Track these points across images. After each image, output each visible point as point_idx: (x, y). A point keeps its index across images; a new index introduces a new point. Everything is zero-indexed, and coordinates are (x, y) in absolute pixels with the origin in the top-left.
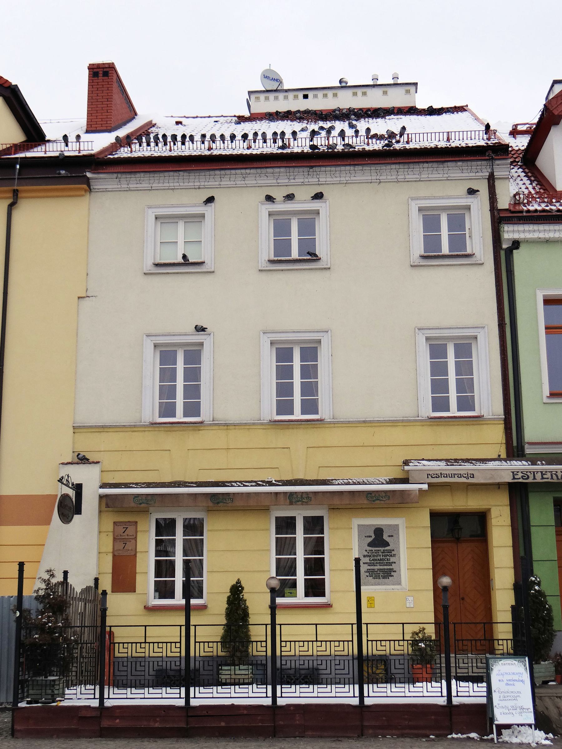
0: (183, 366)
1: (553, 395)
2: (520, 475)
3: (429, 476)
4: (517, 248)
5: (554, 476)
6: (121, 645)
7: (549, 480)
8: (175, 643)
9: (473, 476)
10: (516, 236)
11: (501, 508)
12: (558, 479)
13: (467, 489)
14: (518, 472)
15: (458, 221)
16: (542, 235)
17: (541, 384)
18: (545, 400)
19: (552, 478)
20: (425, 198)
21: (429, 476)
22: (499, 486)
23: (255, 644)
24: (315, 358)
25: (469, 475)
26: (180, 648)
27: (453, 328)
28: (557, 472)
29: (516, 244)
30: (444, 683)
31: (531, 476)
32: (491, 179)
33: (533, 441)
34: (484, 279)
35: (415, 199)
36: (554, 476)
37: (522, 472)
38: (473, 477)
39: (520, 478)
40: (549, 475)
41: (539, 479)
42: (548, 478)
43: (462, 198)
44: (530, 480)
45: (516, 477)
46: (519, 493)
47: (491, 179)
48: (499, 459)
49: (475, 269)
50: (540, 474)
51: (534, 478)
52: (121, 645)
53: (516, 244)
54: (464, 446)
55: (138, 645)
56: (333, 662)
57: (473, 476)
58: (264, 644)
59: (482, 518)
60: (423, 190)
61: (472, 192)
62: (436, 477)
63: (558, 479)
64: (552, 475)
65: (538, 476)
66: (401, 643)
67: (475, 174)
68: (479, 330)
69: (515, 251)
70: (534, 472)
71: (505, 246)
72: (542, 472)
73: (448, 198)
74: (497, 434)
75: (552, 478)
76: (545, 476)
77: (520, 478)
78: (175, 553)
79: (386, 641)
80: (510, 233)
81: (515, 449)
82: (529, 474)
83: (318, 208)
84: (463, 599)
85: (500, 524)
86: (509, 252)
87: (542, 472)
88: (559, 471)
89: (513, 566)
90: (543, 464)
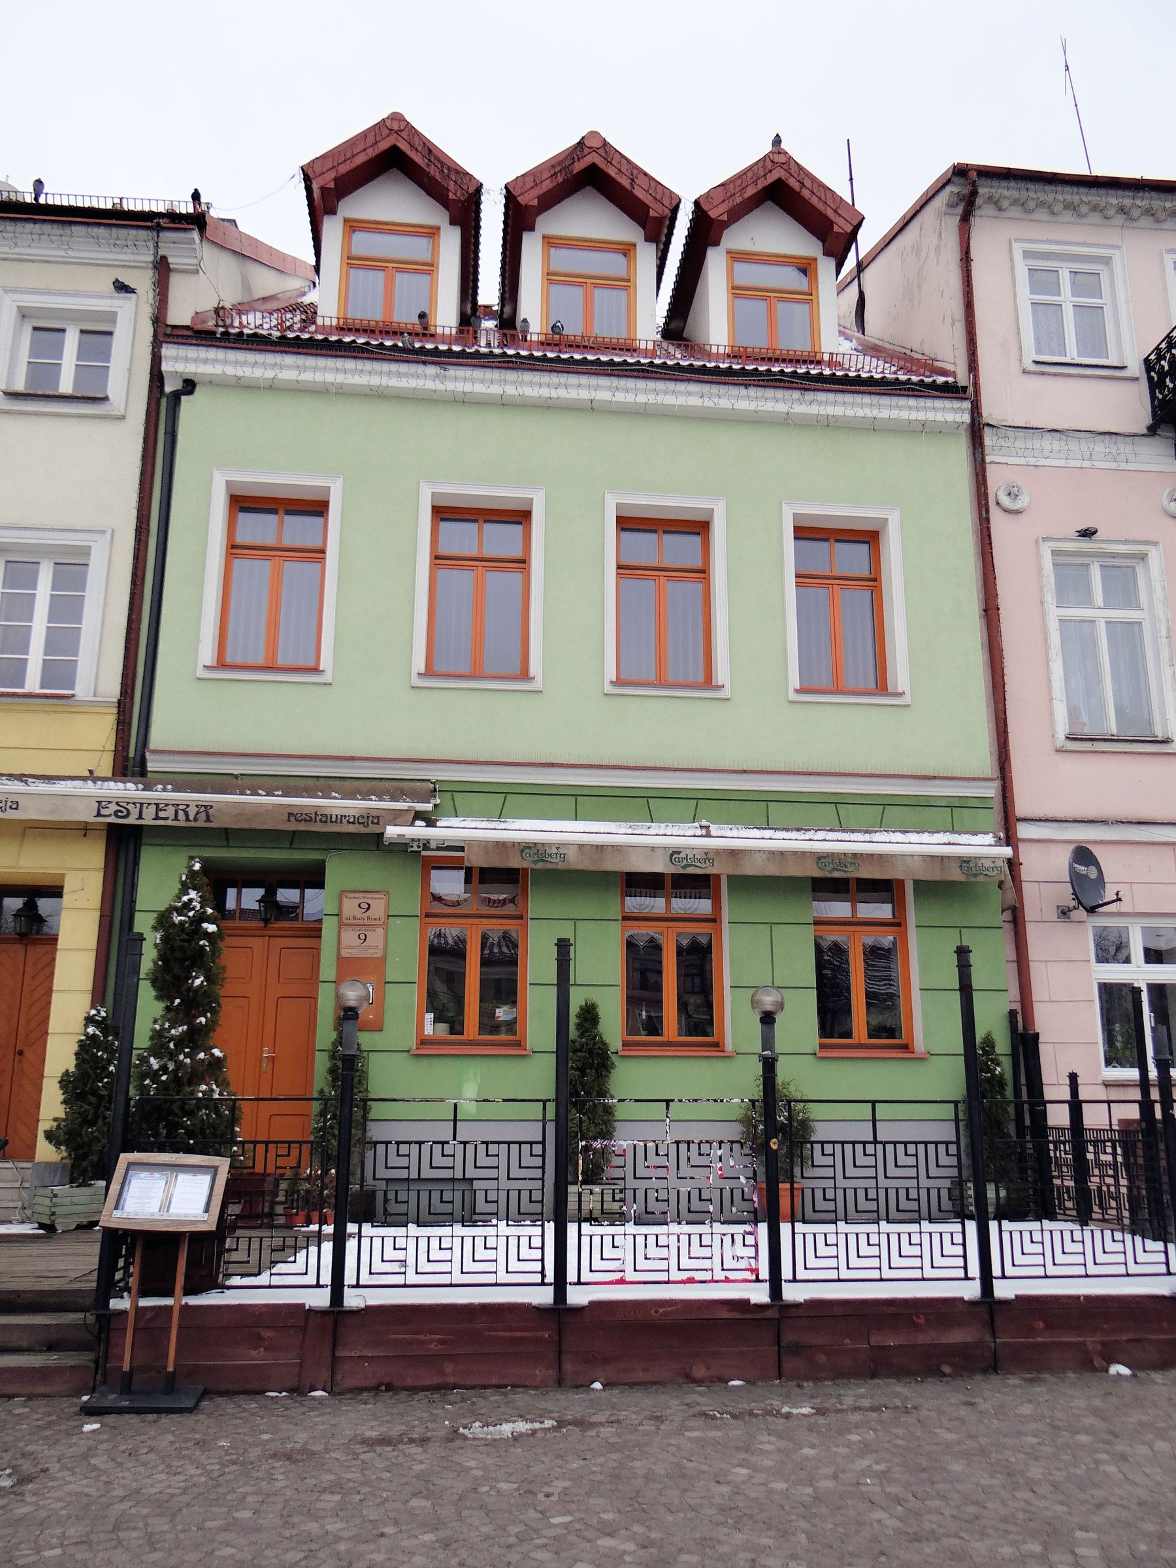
0: (49, 592)
1: (618, 682)
2: (113, 808)
3: (292, 818)
4: (191, 392)
5: (181, 814)
6: (526, 1148)
7: (169, 823)
8: (531, 1143)
9: (16, 806)
10: (190, 369)
11: (85, 873)
12: (187, 819)
13: (23, 835)
14: (167, 805)
15: (98, 336)
16: (230, 371)
17: (198, 641)
18: (608, 688)
19: (176, 819)
20: (31, 292)
21: (292, 818)
22: (84, 829)
23: (381, 1148)
24: (81, 584)
25: (9, 804)
26: (543, 1156)
27: (44, 530)
28: (188, 806)
29: (189, 386)
30: (550, 1227)
31: (135, 812)
32: (162, 268)
33: (181, 749)
34: (119, 446)
35: (10, 291)
36: (181, 815)
37: (117, 803)
38: (378, 823)
39: (110, 816)
40: (170, 812)
41: (148, 819)
42: (167, 819)
43: (101, 297)
44: (131, 820)
45: (103, 812)
46: (124, 842)
47: (162, 268)
48: (92, 777)
49: (106, 428)
50: (153, 808)
51: (140, 817)
52: (392, 1148)
53: (189, 386)
54: (31, 752)
55: (526, 1148)
56: (492, 1184)
57: (16, 806)
58: (538, 1149)
59: (40, 892)
60: (32, 276)
61: (122, 288)
62: (305, 820)
63: (187, 819)
64: (176, 812)
65: (149, 813)
66: (870, 1149)
67: (132, 256)
68: (96, 536)
69: (183, 398)
70: (142, 804)
71: (168, 389)
72: (157, 805)
73: (75, 295)
74: (99, 733)
75: (176, 819)
76: (161, 814)
77: (110, 816)
78: (1159, 985)
79: (499, 1143)
80: (180, 361)
81: (130, 762)
82: (130, 807)
83: (114, 309)
84: (21, 1053)
85: (77, 905)
86: (176, 397)
87: (157, 805)
88: (193, 805)
89: (90, 988)
90: (164, 790)
